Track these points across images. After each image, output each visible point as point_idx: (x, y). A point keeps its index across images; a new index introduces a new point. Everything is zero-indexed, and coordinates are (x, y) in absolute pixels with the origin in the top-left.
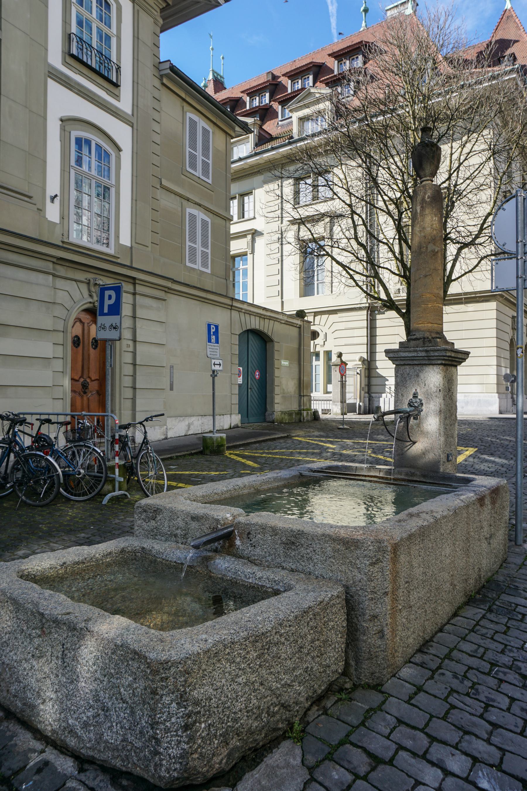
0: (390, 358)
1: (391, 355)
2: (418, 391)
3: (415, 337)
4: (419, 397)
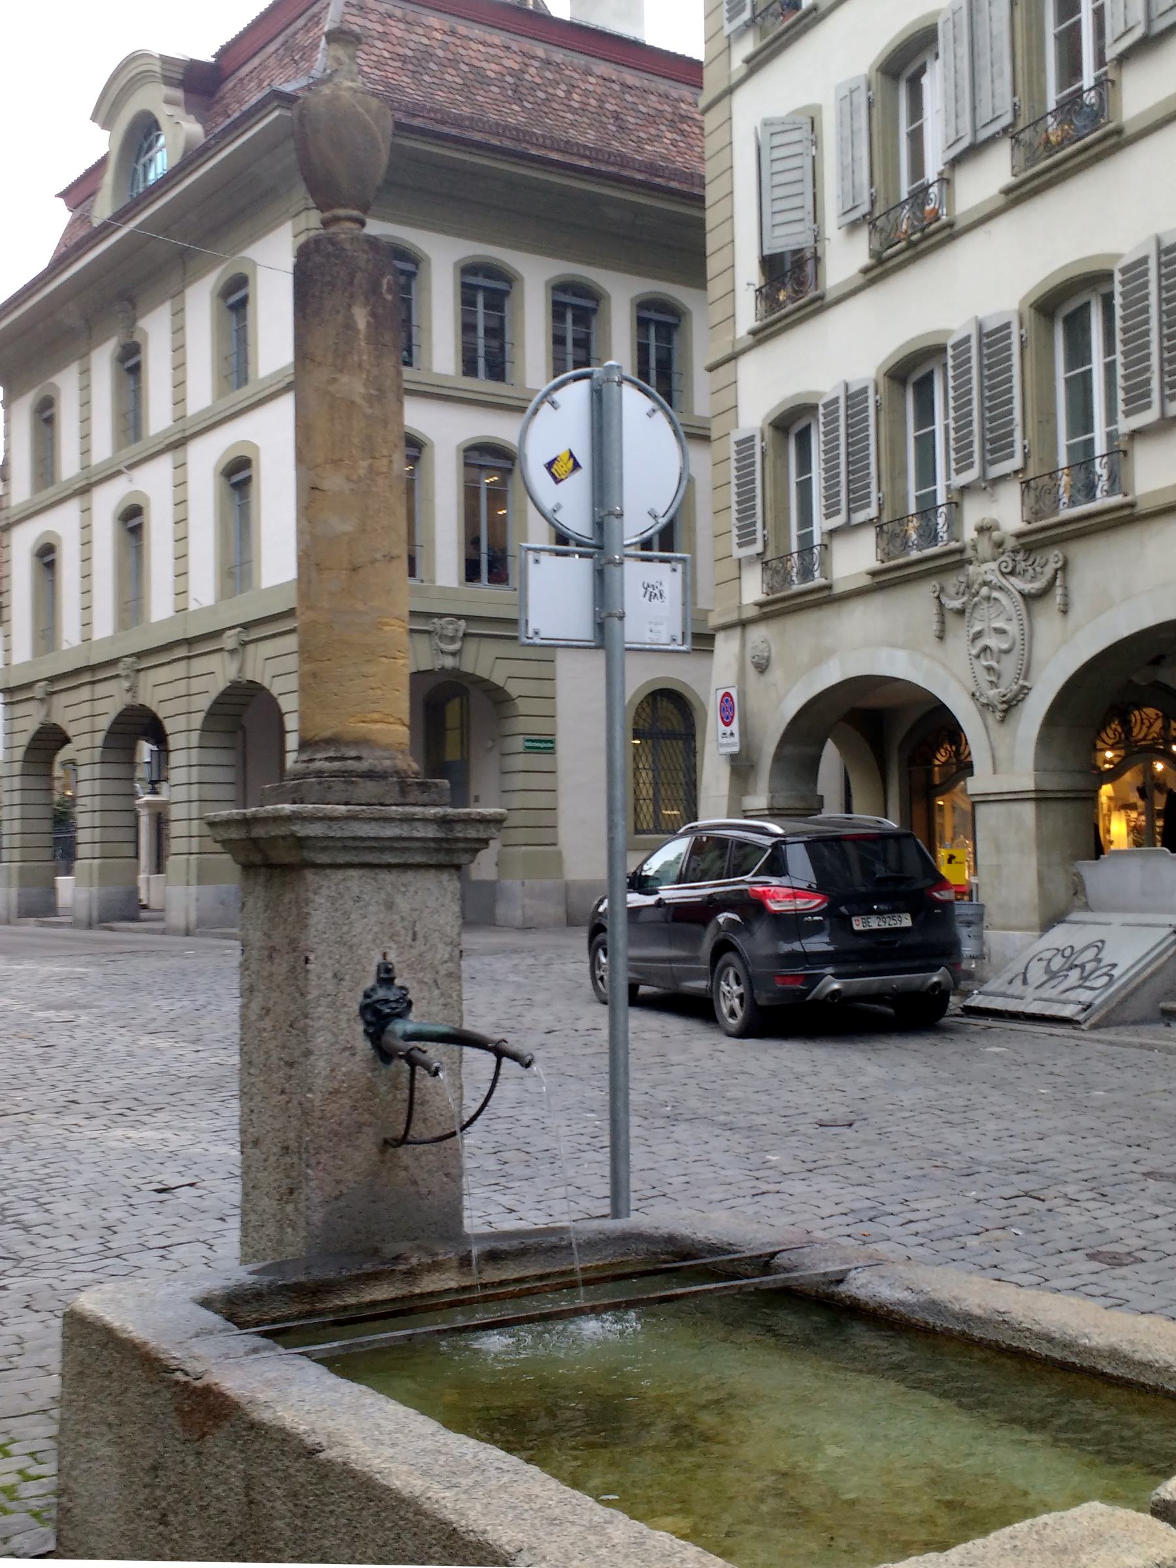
2: (392, 957)
3: (364, 766)
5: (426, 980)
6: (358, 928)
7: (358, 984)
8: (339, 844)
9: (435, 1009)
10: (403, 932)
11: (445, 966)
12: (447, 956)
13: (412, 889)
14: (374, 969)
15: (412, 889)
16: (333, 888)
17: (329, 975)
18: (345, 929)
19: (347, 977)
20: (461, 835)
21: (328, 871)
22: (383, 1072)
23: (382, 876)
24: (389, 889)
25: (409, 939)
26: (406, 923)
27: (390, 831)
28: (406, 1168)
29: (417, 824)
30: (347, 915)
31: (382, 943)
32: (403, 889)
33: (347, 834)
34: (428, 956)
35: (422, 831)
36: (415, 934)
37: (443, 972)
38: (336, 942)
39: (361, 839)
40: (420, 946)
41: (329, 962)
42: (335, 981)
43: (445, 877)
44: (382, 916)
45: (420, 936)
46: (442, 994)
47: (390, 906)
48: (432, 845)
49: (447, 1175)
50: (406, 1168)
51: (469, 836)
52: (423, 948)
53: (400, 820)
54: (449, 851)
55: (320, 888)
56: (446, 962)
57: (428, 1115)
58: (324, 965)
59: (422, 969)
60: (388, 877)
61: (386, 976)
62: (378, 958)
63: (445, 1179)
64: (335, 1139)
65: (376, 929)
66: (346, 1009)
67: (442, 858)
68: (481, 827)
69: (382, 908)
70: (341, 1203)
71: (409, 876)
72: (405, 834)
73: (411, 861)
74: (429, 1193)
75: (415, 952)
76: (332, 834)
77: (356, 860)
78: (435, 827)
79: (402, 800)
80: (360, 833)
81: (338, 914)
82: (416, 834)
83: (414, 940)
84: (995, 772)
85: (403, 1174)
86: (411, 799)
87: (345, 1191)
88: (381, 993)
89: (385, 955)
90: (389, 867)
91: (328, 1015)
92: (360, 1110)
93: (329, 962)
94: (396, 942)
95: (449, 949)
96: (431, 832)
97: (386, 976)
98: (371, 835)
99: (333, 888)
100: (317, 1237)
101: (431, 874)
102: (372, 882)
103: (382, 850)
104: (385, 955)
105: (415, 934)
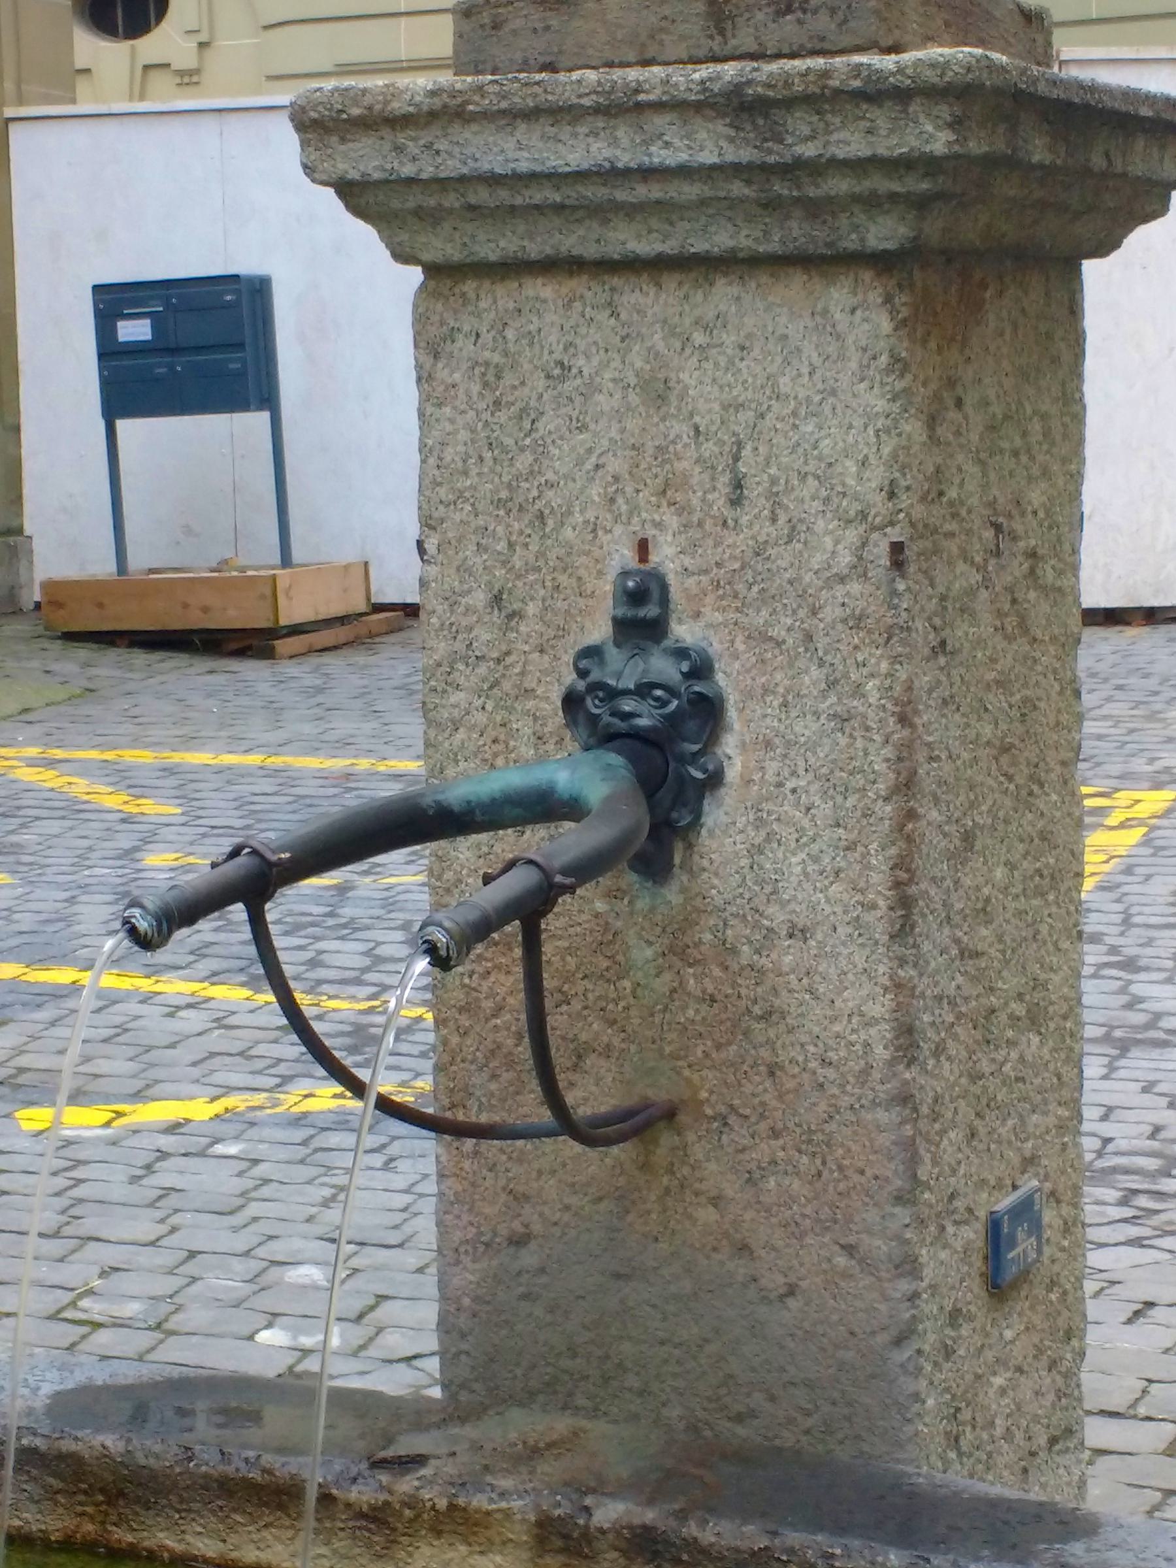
0: (355, 195)
1: (366, 158)
4: (683, 631)
5: (775, 632)
6: (560, 461)
7: (562, 632)
8: (451, 200)
9: (806, 728)
10: (698, 476)
11: (839, 591)
12: (845, 559)
13: (730, 339)
14: (607, 586)
15: (730, 339)
16: (487, 338)
17: (479, 598)
18: (524, 462)
19: (532, 609)
20: (809, 150)
21: (469, 286)
22: (642, 904)
23: (635, 297)
24: (658, 340)
25: (719, 501)
26: (709, 448)
27: (578, 151)
28: (716, 1201)
29: (660, 121)
30: (528, 416)
31: (634, 509)
32: (699, 338)
33: (452, 167)
34: (782, 556)
35: (675, 145)
36: (738, 484)
37: (831, 613)
38: (499, 503)
39: (493, 180)
40: (754, 524)
41: (477, 561)
42: (496, 617)
43: (838, 296)
44: (632, 424)
45: (755, 491)
46: (832, 684)
47: (658, 392)
48: (738, 188)
49: (849, 1250)
50: (716, 1201)
51: (841, 153)
52: (767, 530)
53: (597, 110)
54: (815, 209)
55: (451, 335)
56: (842, 579)
57: (783, 1057)
58: (464, 569)
59: (765, 597)
60: (644, 300)
61: (643, 613)
62: (624, 556)
63: (841, 1260)
64: (507, 1076)
65: (615, 465)
66: (530, 704)
67: (796, 233)
68: (881, 117)
69: (634, 398)
70: (529, 1258)
71: (723, 294)
72: (625, 159)
73: (699, 246)
74: (791, 1291)
75: (741, 541)
76: (408, 170)
77: (535, 250)
78: (721, 127)
79: (716, 45)
80: (493, 163)
81: (502, 416)
82: (660, 156)
83: (736, 502)
84: (366, 564)
85: (707, 1215)
86: (744, 40)
87: (537, 1228)
88: (623, 670)
89: (643, 548)
90: (631, 265)
91: (480, 718)
92: (577, 1005)
93: (477, 561)
94: (682, 509)
95: (852, 535)
96: (709, 144)
97: (643, 613)
98: (524, 166)
99: (487, 338)
100: (463, 1336)
101: (795, 286)
102: (602, 316)
103: (602, 212)
104: (643, 548)
105: (738, 484)
